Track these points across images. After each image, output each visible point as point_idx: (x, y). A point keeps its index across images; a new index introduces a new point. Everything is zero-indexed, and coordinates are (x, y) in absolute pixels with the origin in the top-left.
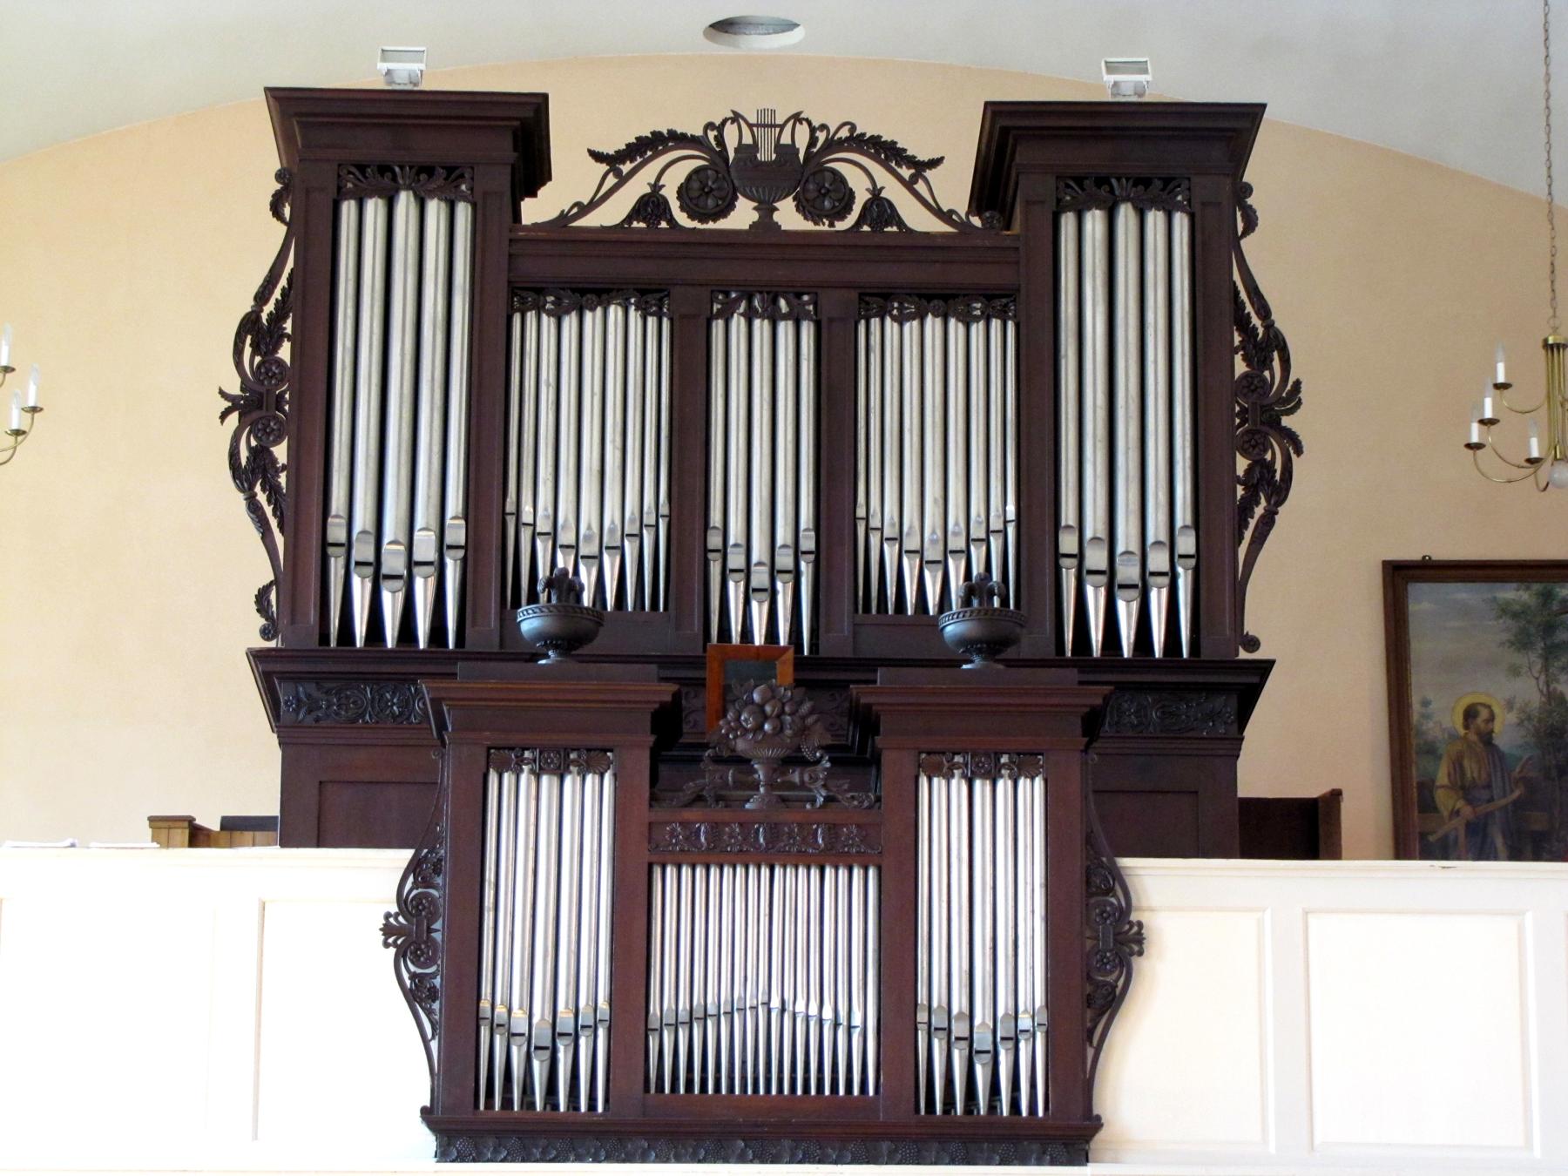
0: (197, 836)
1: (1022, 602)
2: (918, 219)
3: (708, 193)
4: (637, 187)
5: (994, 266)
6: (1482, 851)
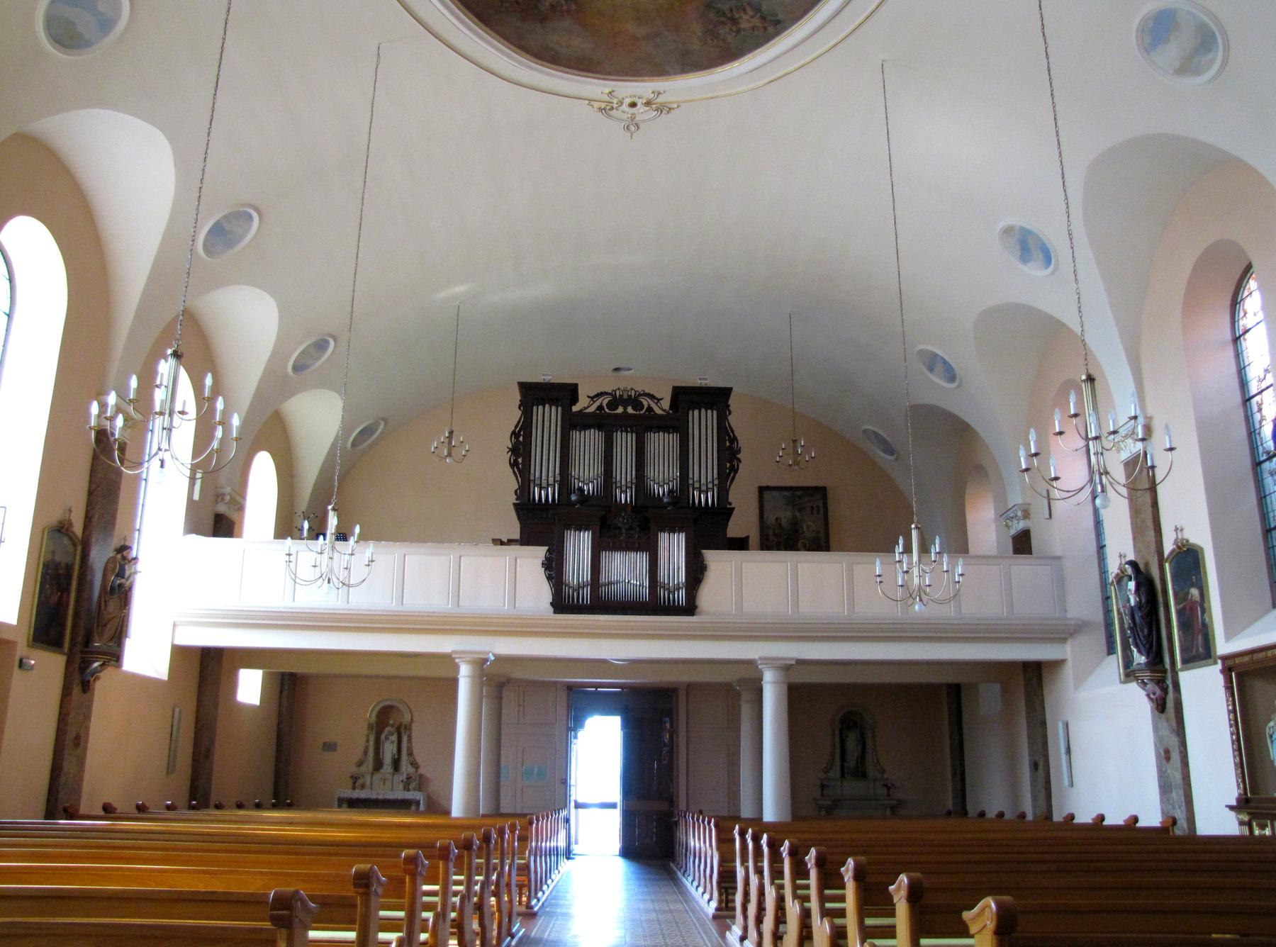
0: (502, 543)
1: (680, 497)
2: (658, 411)
3: (613, 405)
4: (597, 404)
5: (675, 422)
6: (779, 549)
